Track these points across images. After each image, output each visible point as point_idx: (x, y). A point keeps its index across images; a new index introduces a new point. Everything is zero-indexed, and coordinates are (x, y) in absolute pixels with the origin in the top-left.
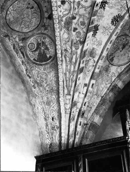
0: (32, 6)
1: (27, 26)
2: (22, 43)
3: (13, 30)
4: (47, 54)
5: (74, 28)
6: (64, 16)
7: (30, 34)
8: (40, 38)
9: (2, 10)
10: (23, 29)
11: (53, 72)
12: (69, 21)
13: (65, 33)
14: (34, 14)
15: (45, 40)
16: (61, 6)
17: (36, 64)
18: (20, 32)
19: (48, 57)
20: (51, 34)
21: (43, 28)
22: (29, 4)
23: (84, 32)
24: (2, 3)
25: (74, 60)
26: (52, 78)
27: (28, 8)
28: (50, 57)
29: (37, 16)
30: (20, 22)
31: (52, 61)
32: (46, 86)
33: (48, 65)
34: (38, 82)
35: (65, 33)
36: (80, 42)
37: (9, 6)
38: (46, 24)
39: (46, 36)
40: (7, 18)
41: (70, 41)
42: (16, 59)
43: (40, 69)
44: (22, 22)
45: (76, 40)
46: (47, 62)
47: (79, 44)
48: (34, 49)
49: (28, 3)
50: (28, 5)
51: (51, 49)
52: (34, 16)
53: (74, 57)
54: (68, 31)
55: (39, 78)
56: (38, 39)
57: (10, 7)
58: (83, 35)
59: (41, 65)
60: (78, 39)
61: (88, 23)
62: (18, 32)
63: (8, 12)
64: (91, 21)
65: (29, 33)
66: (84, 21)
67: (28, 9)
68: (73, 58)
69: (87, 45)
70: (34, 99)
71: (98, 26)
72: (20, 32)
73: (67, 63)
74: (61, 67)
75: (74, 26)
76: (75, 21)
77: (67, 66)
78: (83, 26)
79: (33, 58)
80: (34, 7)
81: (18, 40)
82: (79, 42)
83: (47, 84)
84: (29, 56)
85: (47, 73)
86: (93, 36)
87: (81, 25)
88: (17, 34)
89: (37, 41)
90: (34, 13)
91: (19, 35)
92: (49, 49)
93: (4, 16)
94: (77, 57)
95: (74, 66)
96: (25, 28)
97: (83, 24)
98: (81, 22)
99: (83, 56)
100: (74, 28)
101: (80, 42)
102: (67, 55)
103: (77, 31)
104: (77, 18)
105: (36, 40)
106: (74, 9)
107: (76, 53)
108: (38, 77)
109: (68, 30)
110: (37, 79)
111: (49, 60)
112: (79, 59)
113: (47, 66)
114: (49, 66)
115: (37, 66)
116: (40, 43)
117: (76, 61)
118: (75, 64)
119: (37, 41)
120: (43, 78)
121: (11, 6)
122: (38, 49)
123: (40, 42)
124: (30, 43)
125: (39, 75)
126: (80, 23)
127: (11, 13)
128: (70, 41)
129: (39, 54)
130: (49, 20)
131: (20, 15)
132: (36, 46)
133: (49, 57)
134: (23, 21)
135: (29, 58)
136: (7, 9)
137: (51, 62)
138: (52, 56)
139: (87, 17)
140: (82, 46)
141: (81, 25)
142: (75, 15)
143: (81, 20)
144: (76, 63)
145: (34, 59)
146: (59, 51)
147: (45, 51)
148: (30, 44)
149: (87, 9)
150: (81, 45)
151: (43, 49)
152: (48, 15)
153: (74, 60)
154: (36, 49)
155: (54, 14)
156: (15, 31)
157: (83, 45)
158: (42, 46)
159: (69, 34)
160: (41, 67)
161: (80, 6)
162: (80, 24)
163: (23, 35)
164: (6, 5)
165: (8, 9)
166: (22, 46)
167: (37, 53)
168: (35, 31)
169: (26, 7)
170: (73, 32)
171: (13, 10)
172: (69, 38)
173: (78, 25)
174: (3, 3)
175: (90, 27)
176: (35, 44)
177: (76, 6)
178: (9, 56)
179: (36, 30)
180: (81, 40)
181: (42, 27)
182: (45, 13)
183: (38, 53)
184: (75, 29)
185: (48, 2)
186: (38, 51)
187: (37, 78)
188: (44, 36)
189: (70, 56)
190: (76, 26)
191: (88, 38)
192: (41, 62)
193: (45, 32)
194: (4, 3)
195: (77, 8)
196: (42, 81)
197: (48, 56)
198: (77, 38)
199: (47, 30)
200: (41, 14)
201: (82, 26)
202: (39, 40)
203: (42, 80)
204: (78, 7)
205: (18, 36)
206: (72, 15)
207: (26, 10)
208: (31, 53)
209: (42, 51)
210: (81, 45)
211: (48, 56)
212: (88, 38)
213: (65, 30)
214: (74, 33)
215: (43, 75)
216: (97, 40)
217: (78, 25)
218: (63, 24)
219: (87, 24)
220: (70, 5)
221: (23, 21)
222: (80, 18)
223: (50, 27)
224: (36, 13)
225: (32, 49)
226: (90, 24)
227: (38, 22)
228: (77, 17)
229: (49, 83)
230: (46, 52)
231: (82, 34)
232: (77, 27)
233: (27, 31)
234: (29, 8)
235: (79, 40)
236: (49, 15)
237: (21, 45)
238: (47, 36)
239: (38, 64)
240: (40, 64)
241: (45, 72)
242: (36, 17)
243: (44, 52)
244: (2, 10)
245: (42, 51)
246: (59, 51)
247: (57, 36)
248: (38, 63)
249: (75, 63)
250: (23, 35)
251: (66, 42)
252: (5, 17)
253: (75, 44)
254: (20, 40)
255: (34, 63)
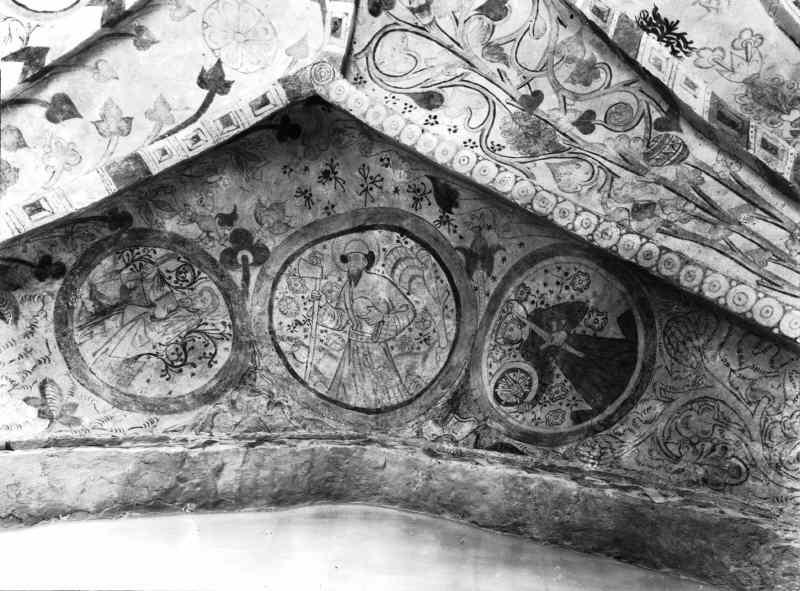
0: (362, 256)
1: (424, 348)
2: (463, 419)
3: (378, 411)
4: (601, 329)
5: (575, 124)
6: (483, 130)
7: (460, 357)
8: (509, 318)
9: (250, 351)
10: (418, 371)
11: (709, 354)
12: (527, 127)
13: (563, 170)
14: (397, 272)
15: (531, 298)
16: (435, 117)
17: (608, 423)
18: (419, 395)
19: (620, 336)
20: (521, 245)
21: (479, 274)
22: (344, 259)
23: (627, 84)
24: (224, 323)
25: (730, 201)
26: (737, 382)
27: (355, 279)
28: (626, 322)
29: (413, 267)
30: (377, 361)
31: (649, 326)
32: (765, 444)
33: (659, 361)
34: (701, 472)
35: (563, 170)
36: (660, 125)
37: (265, 319)
38: (468, 245)
39: (519, 281)
40: (300, 372)
41: (616, 169)
42: (481, 483)
43: (646, 422)
44: (386, 352)
45: (637, 138)
46: (640, 356)
47: (668, 135)
48: (530, 386)
49: (338, 260)
50: (345, 266)
51: (588, 293)
52: (406, 279)
53: (711, 188)
54: (566, 154)
55: (688, 455)
56: (508, 333)
57: (271, 320)
58: (640, 96)
59: (632, 401)
60: (640, 130)
61: (598, 47)
62: (410, 402)
63: (284, 346)
64: (591, 16)
65: (455, 359)
66: (580, 61)
67: (361, 282)
68: (714, 197)
69: (693, 86)
70: (357, 153)
71: (656, 15)
72: (419, 395)
73: (713, 241)
74: (699, 273)
75: (565, 122)
76: (549, 105)
77: (727, 251)
78: (597, 76)
79: (567, 417)
80: (371, 253)
81: (437, 430)
82: (655, 133)
83: (756, 434)
84: (541, 429)
85: (691, 396)
86: (681, 54)
87: (587, 84)
88: (411, 412)
89: (512, 343)
90: (394, 267)
91: (423, 410)
92: (581, 297)
93: (281, 369)
94: (726, 174)
95: (760, 218)
96: (419, 360)
97: (587, 73)
98: (575, 78)
99: (733, 131)
100: (575, 124)
101: (660, 125)
102: (673, 217)
103: (600, 117)
104: (545, 92)
105: (506, 348)
106: (498, 80)
107: (700, 168)
108: (678, 459)
109: (558, 150)
110: (678, 472)
111: (636, 343)
112: (744, 175)
113: (663, 370)
114: (663, 360)
115: (621, 430)
116: (532, 333)
117: (741, 190)
118: (756, 206)
119: (512, 343)
120: (706, 436)
121: (276, 313)
122: (548, 363)
123: (526, 330)
124: (493, 385)
125: (671, 447)
126: (574, 82)
127: (298, 343)
128: (616, 169)
129: (570, 375)
130: (454, 210)
131: (347, 329)
132: (527, 367)
133: (623, 333)
134: (390, 344)
135: (545, 436)
136: (269, 336)
137: (654, 336)
138: (621, 309)
139: (569, 38)
140: (684, 127)
141: (587, 84)
142: (525, 91)
143: (564, 72)
144: (757, 196)
145: (578, 418)
146: (604, 233)
147: (579, 330)
148: (496, 386)
149: (539, 24)
150: (681, 131)
151: (563, 334)
152: (431, 197)
153: (730, 201)
154: (541, 376)
155: (430, 149)
156: (393, 408)
157: (685, 118)
158: (549, 330)
159: (578, 158)
160: (640, 407)
161: (508, 49)
162: (579, 89)
163: (439, 390)
164: (249, 324)
165: (272, 332)
166: (474, 432)
167: (559, 379)
168: (469, 329)
169: (345, 279)
170: (589, 138)
171: (298, 323)
172: (601, 166)
173: (576, 97)
174: (229, 321)
175: (616, 32)
176: (515, 365)
177: (493, 67)
178: (447, 516)
179: (467, 315)
180: (656, 115)
181: (470, 273)
182: (418, 213)
183: (563, 378)
184: (586, 123)
185: (387, 166)
186: (558, 371)
187: (676, 467)
188: (510, 293)
189: (690, 207)
190: (575, 111)
191: (659, 68)
192: (623, 389)
193: (500, 269)
194: (233, 318)
195: (503, 67)
196: (713, 450)
197: (613, 331)
198: (629, 134)
199: (498, 257)
200: (413, 238)
201: (596, 85)
202: (517, 333)
203: (708, 445)
204: (504, 58)
205: (422, 418)
206: (513, 98)
207: (355, 290)
208: (538, 407)
209: (572, 350)
210: (681, 131)
211: (613, 331)
212: (659, 68)
213: (548, 164)
214: (599, 135)
215: (687, 426)
216: (722, 50)
217: (576, 97)
218: (516, 153)
219: (602, 53)
220: (467, 84)
221: (385, 341)
222: (553, 72)
223: (489, 228)
224: (398, 261)
225: (526, 395)
226: (599, 23)
227: (438, 278)
228: (542, 84)
229: (757, 419)
230: (589, 332)
231: (629, 99)
232: (582, 107)
233: (442, 364)
234: (360, 275)
235: (648, 130)
236: (437, 200)
237: (467, 427)
238: (521, 274)
239: (611, 417)
240: (624, 403)
241: (681, 399)
242: (418, 272)
243: (580, 341)
244: (250, 351)
245: (572, 350)
246: (604, 233)
247: (528, 200)
248: (610, 410)
249: (753, 201)
250: (439, 390)
251: (607, 187)
252: (287, 374)
253: (647, 156)
254: (442, 421)
255: (596, 432)
